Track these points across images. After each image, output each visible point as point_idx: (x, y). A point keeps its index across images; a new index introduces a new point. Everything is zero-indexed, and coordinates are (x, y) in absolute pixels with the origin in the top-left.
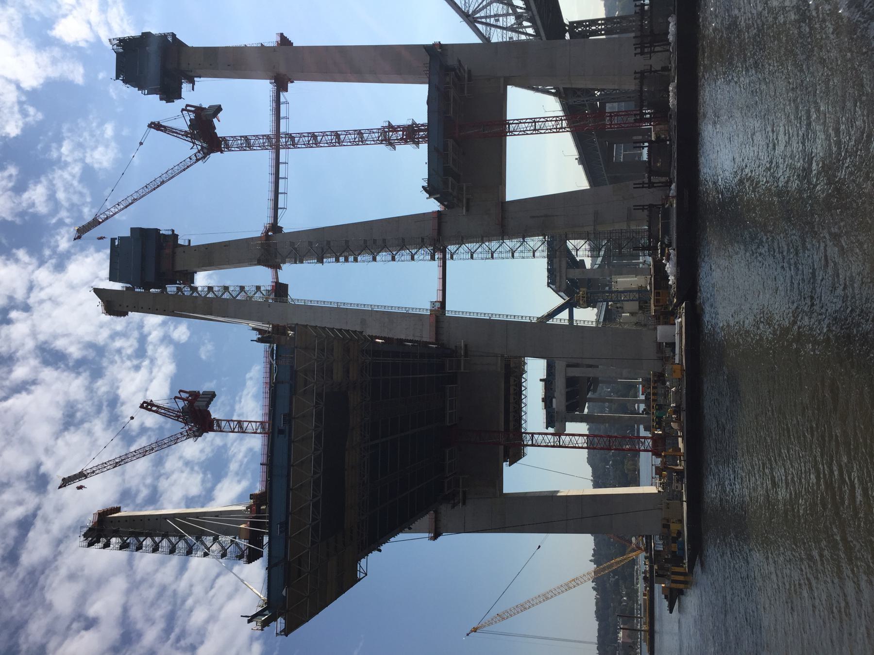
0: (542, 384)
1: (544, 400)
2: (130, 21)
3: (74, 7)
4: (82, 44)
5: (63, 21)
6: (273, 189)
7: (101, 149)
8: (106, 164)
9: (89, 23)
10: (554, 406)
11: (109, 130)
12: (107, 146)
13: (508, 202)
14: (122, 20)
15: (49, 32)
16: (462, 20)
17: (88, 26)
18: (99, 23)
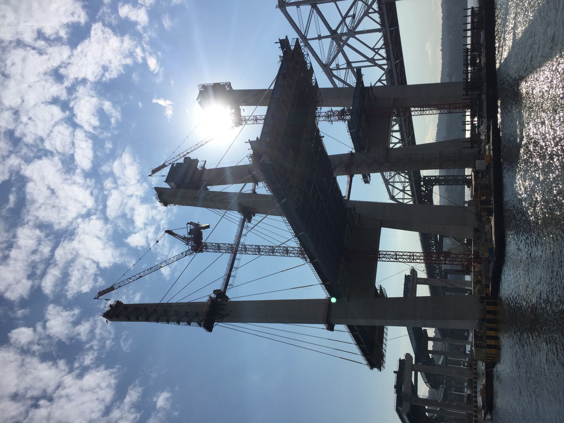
3: (141, 229)
4: (139, 248)
5: (133, 235)
9: (147, 238)
10: (403, 390)
15: (124, 240)
17: (146, 239)
18: (152, 239)
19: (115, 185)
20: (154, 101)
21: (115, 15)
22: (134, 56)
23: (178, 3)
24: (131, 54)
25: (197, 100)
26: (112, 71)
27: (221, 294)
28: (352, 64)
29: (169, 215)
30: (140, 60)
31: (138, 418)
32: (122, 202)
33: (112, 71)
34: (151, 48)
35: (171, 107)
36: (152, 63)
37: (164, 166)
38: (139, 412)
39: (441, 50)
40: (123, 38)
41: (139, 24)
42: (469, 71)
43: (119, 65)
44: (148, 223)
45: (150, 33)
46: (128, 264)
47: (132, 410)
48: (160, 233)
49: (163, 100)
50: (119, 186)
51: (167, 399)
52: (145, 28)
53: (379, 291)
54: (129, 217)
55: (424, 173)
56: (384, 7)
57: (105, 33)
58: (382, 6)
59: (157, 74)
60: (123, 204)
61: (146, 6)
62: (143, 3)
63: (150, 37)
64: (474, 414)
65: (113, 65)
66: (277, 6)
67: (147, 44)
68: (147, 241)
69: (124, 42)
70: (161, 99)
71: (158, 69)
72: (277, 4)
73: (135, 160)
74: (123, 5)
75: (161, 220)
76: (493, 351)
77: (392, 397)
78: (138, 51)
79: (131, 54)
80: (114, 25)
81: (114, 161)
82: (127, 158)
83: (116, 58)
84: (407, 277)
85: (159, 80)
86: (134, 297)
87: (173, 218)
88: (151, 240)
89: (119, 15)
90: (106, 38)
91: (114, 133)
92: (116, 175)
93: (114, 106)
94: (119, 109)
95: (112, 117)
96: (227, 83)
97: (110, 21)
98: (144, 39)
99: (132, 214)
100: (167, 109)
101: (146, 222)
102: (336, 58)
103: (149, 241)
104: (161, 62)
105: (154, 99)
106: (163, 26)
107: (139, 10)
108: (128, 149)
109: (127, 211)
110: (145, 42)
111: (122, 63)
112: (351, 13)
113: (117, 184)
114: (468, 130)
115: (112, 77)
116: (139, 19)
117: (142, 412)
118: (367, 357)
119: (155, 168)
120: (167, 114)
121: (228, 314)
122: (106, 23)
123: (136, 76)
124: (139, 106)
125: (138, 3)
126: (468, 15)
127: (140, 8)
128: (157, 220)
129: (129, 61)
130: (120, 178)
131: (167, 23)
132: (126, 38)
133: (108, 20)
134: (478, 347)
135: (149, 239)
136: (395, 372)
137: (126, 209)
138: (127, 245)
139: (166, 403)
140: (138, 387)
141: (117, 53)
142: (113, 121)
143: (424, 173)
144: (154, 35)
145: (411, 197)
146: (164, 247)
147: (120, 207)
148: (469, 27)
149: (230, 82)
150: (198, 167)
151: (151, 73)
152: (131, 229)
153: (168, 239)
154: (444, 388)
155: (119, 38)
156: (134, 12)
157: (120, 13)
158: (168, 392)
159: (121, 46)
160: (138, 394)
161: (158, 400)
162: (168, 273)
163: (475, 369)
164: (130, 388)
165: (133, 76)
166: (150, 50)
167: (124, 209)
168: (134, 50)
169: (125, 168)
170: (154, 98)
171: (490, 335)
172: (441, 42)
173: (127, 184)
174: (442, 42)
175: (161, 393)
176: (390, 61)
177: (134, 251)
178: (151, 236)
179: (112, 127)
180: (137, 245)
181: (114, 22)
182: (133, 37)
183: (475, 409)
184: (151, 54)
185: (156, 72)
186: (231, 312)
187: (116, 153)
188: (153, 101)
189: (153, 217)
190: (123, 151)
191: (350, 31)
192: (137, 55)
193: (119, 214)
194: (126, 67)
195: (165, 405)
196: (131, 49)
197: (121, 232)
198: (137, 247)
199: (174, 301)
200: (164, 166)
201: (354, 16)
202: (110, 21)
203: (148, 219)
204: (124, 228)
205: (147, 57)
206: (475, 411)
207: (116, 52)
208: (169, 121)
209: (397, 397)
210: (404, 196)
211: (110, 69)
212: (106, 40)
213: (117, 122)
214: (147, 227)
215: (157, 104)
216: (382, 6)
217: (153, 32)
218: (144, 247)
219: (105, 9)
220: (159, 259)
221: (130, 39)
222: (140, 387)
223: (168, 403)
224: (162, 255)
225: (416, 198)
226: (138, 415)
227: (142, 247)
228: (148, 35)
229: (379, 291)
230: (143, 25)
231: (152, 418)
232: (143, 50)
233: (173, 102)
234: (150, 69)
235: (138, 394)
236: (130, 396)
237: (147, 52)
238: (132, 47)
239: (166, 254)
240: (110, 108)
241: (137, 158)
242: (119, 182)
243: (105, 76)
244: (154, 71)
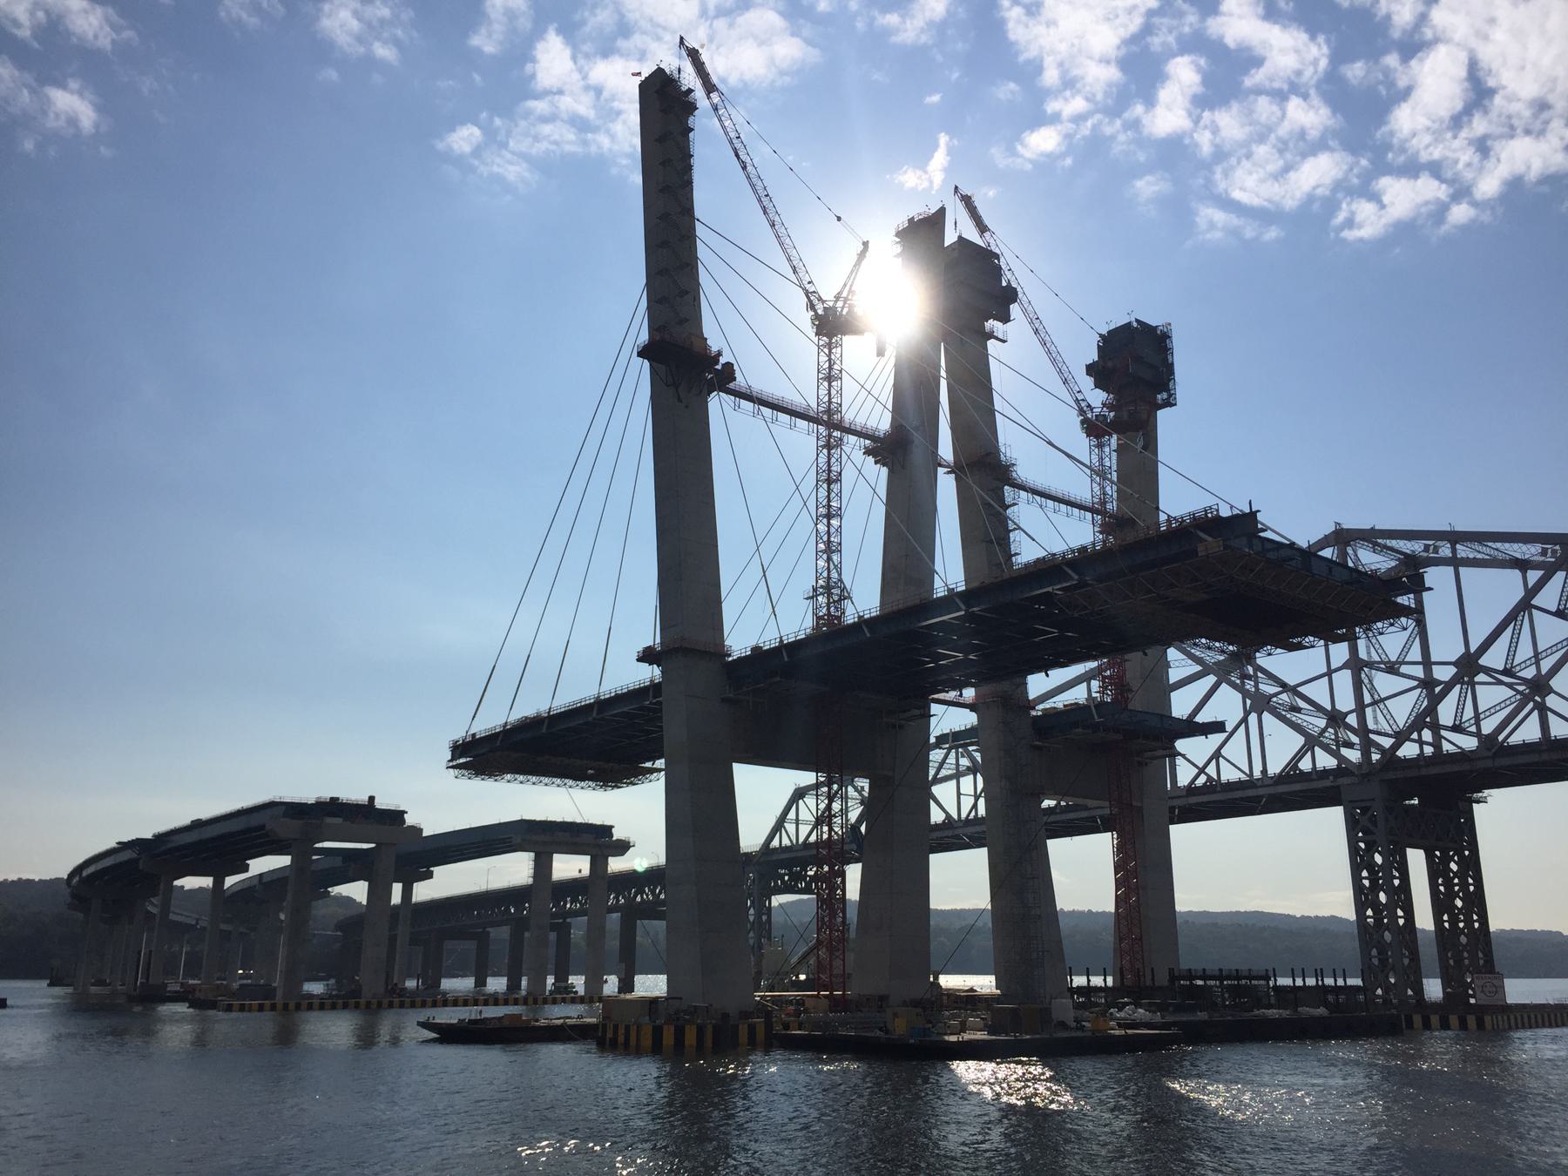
0: (362, 798)
1: (334, 800)
2: (552, 155)
3: (585, 78)
4: (529, 67)
5: (568, 52)
6: (1053, 493)
7: (355, 24)
8: (326, 23)
9: (560, 92)
10: (329, 820)
11: (383, 51)
12: (359, 39)
13: (211, 876)
14: (556, 143)
15: (555, 25)
16: (549, 819)
17: (555, 90)
18: (557, 107)
19: (712, 12)
20: (943, 139)
21: (1174, 46)
22: (1065, 89)
23: (1198, 219)
24: (1069, 84)
25: (1137, 320)
26: (1027, 26)
27: (724, 378)
28: (1085, 684)
29: (624, 162)
30: (1052, 106)
31: (15, 31)
32: (665, 28)
33: (1027, 26)
34: (1084, 138)
35: (926, 184)
36: (1044, 141)
37: (982, 228)
38: (35, 36)
39: (1074, 910)
40: (1113, 64)
41: (1147, 111)
42: (1320, 983)
43: (1041, 48)
44: (602, 98)
45: (1122, 138)
46: (483, 31)
47: (41, 15)
48: (573, 130)
49: (946, 164)
50: (708, 23)
51: (73, 121)
52: (1135, 125)
53: (648, 765)
54: (621, 43)
55: (854, 873)
56: (1327, 783)
57: (1130, 14)
58: (1331, 778)
59: (1012, 152)
60: (660, 31)
61: (1195, 131)
62: (1202, 123)
63: (1113, 138)
64: (363, 1001)
65: (1041, 29)
66: (1339, 524)
67: (1095, 128)
68: (547, 93)
69: (1103, 65)
70: (949, 158)
71: (1028, 154)
72: (1345, 527)
73: (782, 73)
74: (1199, 69)
75: (613, 137)
76: (647, 1041)
77: (307, 791)
78: (1077, 105)
79: (1069, 84)
80: (1149, 39)
81: (781, 13)
82: (789, 50)
83: (1061, 41)
84: (606, 830)
85: (997, 154)
86: (385, 42)
87: (614, 171)
88: (552, 103)
89: (1174, 55)
90: (1117, 16)
91: (859, 18)
92: (740, 15)
93: (931, 24)
94: (924, 39)
95: (903, 16)
96: (1175, 398)
97: (1159, 29)
98: (1107, 120)
99: (628, 55)
100: (919, 173)
101: (605, 94)
102: (1190, 662)
103: (548, 98)
104: (1046, 163)
105: (947, 138)
106: (1140, 176)
107: (1183, 113)
108: (814, 55)
109: (637, 40)
110: (1100, 123)
111: (1046, 56)
112: (1302, 704)
113: (716, 17)
114: (1089, 981)
115: (1011, 25)
116: (1160, 110)
117: (36, 45)
118: (501, 736)
119: (976, 204)
120: (905, 172)
121: (680, 400)
122: (1156, 20)
123: (1012, 92)
124: (930, 94)
125: (1203, 111)
126: (1347, 980)
127: (1190, 114)
128: (611, 125)
129: (1051, 76)
130: (731, 25)
131: (1147, 187)
132: (1112, 73)
133: (1161, 24)
134: (650, 1005)
135: (557, 97)
136: (372, 799)
137: (644, 37)
138: (538, 33)
139: (63, 117)
140: (114, 36)
141: (1073, 45)
142: (892, 19)
143: (854, 873)
144: (1117, 149)
145: (801, 840)
146: (530, 139)
147: (651, 20)
148: (1329, 981)
149: (1175, 404)
150: (991, 321)
151: (1017, 137)
152: (586, 48)
153: (554, 152)
154: (197, 923)
155: (1113, 53)
156: (1180, 98)
157: (1179, 60)
158: (97, 126)
159: (1091, 58)
160: (91, 35)
161: (72, 92)
162: (455, 147)
163: (391, 1005)
164: (110, 11)
165: (1012, 86)
166: (1078, 136)
167: (644, 33)
168: (1079, 92)
169: (761, 43)
170: (951, 139)
171: (665, 1033)
172: (1081, 909)
173: (714, 47)
174: (1081, 913)
175: (91, 102)
176: (1185, 793)
177: (520, 53)
178: (566, 103)
179: (877, 14)
180: (538, 62)
181: (1156, 42)
182: (1114, 89)
183: (292, 1006)
184: (1068, 137)
185: (1019, 147)
186: (687, 407)
187: (801, 21)
188: (943, 134)
189: (619, 113)
190: (809, 42)
191: (1266, 701)
192: (1066, 100)
193: (631, 17)
194: (1037, 67)
195: (57, 116)
196: (1084, 86)
197: (577, 17)
198: (534, 60)
199: (702, 252)
200: (982, 228)
201: (1298, 710)
202: (1159, 29)
203: (613, 98)
204: (587, 29)
205: (1059, 127)
206: (368, 1005)
207: (1076, 42)
208: (888, 177)
209: (306, 804)
210: (806, 823)
211: (1031, 23)
212: (1110, 17)
213: (888, 32)
214: (592, 93)
215: (936, 147)
216: (1331, 778)
217: (1124, 147)
218: (533, 82)
219: (1192, 18)
220: (498, 122)
221: (1110, 85)
222: (113, 42)
223: (62, 122)
224: (509, 133)
225: (800, 854)
226: (25, 33)
227: (533, 76)
228: (1118, 132)
229: (648, 765)
230: (1144, 121)
231: (17, 73)
232: (1079, 119)
233: (937, 191)
234: (1028, 133)
235: (91, 35)
236: (86, 12)
237: (1074, 126)
238: (1088, 88)
239: (511, 144)
240: (928, 14)
241: (787, 79)
242: (721, 24)
243: (1012, 6)
244: (1022, 144)
